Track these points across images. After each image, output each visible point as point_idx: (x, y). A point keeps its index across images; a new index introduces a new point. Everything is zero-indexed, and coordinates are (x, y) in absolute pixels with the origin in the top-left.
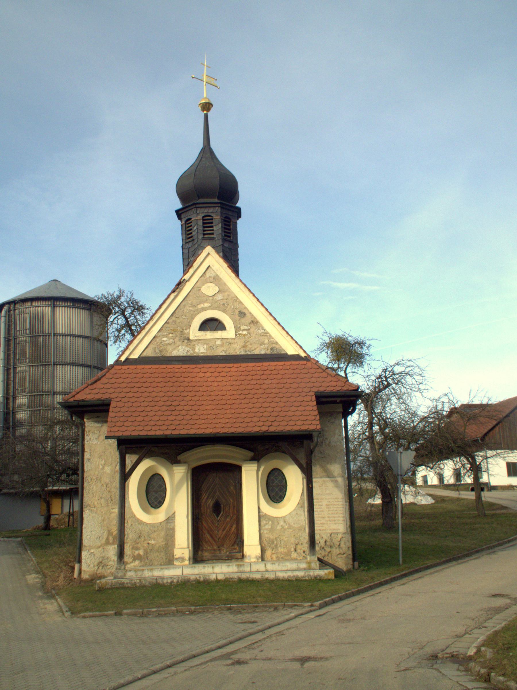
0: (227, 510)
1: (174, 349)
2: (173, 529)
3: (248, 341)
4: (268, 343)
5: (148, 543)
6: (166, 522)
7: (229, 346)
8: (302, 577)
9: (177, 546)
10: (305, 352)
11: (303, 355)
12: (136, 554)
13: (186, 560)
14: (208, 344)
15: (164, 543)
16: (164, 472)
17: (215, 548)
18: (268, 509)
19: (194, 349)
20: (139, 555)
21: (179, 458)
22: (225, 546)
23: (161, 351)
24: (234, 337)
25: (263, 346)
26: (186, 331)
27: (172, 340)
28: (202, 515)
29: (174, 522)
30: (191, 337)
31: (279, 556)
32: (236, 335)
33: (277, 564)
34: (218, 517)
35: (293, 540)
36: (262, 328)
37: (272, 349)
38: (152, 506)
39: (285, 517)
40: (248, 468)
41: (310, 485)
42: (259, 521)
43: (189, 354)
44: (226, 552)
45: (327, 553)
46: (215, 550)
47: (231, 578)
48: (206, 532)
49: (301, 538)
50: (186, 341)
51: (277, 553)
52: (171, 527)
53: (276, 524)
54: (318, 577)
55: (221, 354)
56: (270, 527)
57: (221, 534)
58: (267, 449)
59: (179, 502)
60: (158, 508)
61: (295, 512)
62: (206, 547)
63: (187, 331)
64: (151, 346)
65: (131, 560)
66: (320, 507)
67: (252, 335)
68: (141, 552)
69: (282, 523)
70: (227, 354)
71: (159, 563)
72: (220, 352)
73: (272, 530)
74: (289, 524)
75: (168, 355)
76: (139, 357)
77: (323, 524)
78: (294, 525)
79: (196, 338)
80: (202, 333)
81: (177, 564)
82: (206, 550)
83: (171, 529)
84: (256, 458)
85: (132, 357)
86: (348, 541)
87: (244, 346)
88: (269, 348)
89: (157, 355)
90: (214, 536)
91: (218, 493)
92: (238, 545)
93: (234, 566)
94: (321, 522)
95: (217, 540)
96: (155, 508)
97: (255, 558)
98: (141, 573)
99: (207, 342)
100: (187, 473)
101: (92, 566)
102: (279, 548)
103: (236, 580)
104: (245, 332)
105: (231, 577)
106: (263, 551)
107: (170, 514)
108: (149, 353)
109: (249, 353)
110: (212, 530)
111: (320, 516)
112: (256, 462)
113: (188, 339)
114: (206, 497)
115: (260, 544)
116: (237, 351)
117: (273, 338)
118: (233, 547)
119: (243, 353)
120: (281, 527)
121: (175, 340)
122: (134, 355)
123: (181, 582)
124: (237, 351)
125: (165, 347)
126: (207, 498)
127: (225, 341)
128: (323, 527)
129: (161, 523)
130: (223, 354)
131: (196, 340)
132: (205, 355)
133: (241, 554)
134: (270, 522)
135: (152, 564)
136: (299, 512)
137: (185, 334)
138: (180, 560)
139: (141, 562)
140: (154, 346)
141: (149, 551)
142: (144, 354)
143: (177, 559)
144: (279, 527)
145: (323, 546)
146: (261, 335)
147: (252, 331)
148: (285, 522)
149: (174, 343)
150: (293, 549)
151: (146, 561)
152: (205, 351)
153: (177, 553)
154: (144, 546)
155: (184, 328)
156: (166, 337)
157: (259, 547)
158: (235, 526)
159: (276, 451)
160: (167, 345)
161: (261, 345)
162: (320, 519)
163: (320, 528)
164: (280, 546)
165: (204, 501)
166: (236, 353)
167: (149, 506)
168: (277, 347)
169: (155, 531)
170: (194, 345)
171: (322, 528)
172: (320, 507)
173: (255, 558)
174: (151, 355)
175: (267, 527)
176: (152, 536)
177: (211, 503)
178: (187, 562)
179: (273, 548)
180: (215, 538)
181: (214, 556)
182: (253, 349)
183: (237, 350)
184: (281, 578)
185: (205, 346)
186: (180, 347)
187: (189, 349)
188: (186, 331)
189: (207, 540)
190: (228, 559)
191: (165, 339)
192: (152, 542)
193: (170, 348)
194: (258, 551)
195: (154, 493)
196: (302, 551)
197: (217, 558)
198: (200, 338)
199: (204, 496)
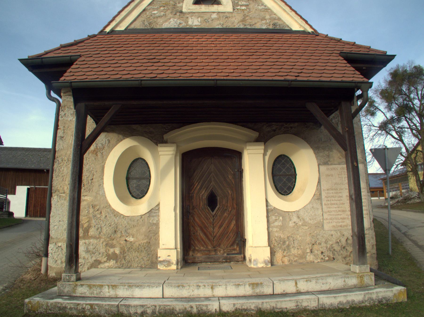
1: (166, 21)
2: (157, 225)
3: (247, 16)
4: (270, 19)
5: (126, 240)
6: (148, 215)
7: (227, 19)
8: (360, 302)
9: (161, 246)
10: (311, 27)
11: (310, 30)
12: (110, 253)
13: (172, 263)
14: (202, 17)
15: (145, 241)
16: (147, 155)
17: (210, 248)
18: (278, 202)
19: (187, 22)
20: (114, 253)
21: (166, 137)
22: (222, 246)
23: (150, 24)
24: (232, 11)
25: (263, 22)
26: (178, 5)
27: (162, 13)
28: (193, 209)
29: (159, 216)
30: (184, 10)
31: (292, 259)
32: (234, 9)
33: (314, 281)
34: (213, 211)
35: (308, 239)
36: (263, 4)
37: (274, 24)
38: (133, 196)
39: (298, 211)
40: (249, 151)
41: (355, 163)
42: (268, 217)
43: (181, 26)
44: (224, 253)
45: (349, 253)
46: (209, 251)
47: (245, 310)
48: (198, 229)
49: (319, 237)
50: (178, 14)
51: (289, 255)
52: (155, 222)
53: (288, 220)
54: (384, 301)
55: (217, 27)
56: (280, 224)
57: (217, 231)
58: (275, 131)
59: (165, 194)
60: (141, 198)
61: (311, 205)
62: (199, 247)
63: (181, 5)
64: (140, 19)
65: (105, 259)
66: (339, 199)
67: (251, 10)
68: (117, 251)
69: (295, 219)
70: (224, 26)
71: (139, 265)
72: (216, 25)
73: (282, 228)
74: (304, 220)
75: (158, 27)
76: (125, 29)
77: (344, 218)
78: (309, 222)
79: (189, 11)
80: (197, 6)
81: (161, 268)
82: (198, 251)
83: (153, 224)
84: (263, 139)
85: (118, 29)
86: (373, 238)
87: (243, 20)
88: (271, 23)
89: (146, 28)
90: (208, 234)
91: (213, 183)
92: (238, 245)
93: (247, 286)
94: (342, 216)
95: (212, 238)
96: (136, 198)
97: (262, 263)
98: (98, 290)
99: (202, 15)
100: (176, 156)
101: (59, 262)
102: (292, 250)
103: (254, 312)
104: (243, 8)
105: (245, 307)
106: (273, 253)
107: (154, 206)
108: (138, 25)
109: (249, 27)
110: (205, 227)
111: (340, 209)
112: (263, 143)
113: (181, 12)
114: (198, 187)
115: (269, 245)
116: (235, 24)
117: (275, 14)
118: (232, 248)
119: (242, 27)
120: (294, 224)
121: (167, 13)
122: (121, 27)
123: (160, 313)
124: (235, 24)
125: (155, 20)
126: (200, 188)
127: (221, 15)
128: (344, 222)
129: (141, 216)
130: (220, 27)
131: (190, 13)
132: (200, 27)
133: (243, 255)
134: (281, 218)
135: (131, 266)
136: (315, 205)
137: (178, 7)
138: (165, 264)
139: (117, 262)
140: (143, 19)
141: (126, 250)
142: (132, 27)
143: (161, 262)
144: (291, 224)
145: (344, 245)
146: (261, 10)
147: (251, 6)
148: (298, 217)
149: (165, 15)
150: (308, 251)
151: (123, 262)
152: (199, 24)
153: (162, 255)
154: (120, 244)
155: (177, 2)
156: (157, 10)
157: (269, 248)
158: (234, 222)
159: (285, 133)
160: (157, 18)
161: (262, 20)
162: (340, 213)
163: (341, 224)
164: (293, 247)
165: (196, 192)
166: (235, 26)
167: (130, 196)
168: (280, 22)
169: (134, 226)
170: (187, 18)
171: (344, 224)
172: (339, 199)
173: (262, 263)
174: (139, 28)
175: (276, 224)
176: (130, 231)
177: (204, 194)
178: (174, 267)
179: (285, 250)
180: (210, 237)
181: (209, 258)
182: (253, 23)
183: (235, 22)
184: (327, 307)
185: (199, 19)
186: (172, 20)
187: (181, 22)
188: (178, 5)
189: (199, 238)
190: (226, 262)
191: (155, 12)
192: (131, 239)
193: (160, 21)
194: (266, 254)
195: (135, 181)
196: (319, 253)
197: (213, 260)
198: (194, 11)
199: (197, 186)
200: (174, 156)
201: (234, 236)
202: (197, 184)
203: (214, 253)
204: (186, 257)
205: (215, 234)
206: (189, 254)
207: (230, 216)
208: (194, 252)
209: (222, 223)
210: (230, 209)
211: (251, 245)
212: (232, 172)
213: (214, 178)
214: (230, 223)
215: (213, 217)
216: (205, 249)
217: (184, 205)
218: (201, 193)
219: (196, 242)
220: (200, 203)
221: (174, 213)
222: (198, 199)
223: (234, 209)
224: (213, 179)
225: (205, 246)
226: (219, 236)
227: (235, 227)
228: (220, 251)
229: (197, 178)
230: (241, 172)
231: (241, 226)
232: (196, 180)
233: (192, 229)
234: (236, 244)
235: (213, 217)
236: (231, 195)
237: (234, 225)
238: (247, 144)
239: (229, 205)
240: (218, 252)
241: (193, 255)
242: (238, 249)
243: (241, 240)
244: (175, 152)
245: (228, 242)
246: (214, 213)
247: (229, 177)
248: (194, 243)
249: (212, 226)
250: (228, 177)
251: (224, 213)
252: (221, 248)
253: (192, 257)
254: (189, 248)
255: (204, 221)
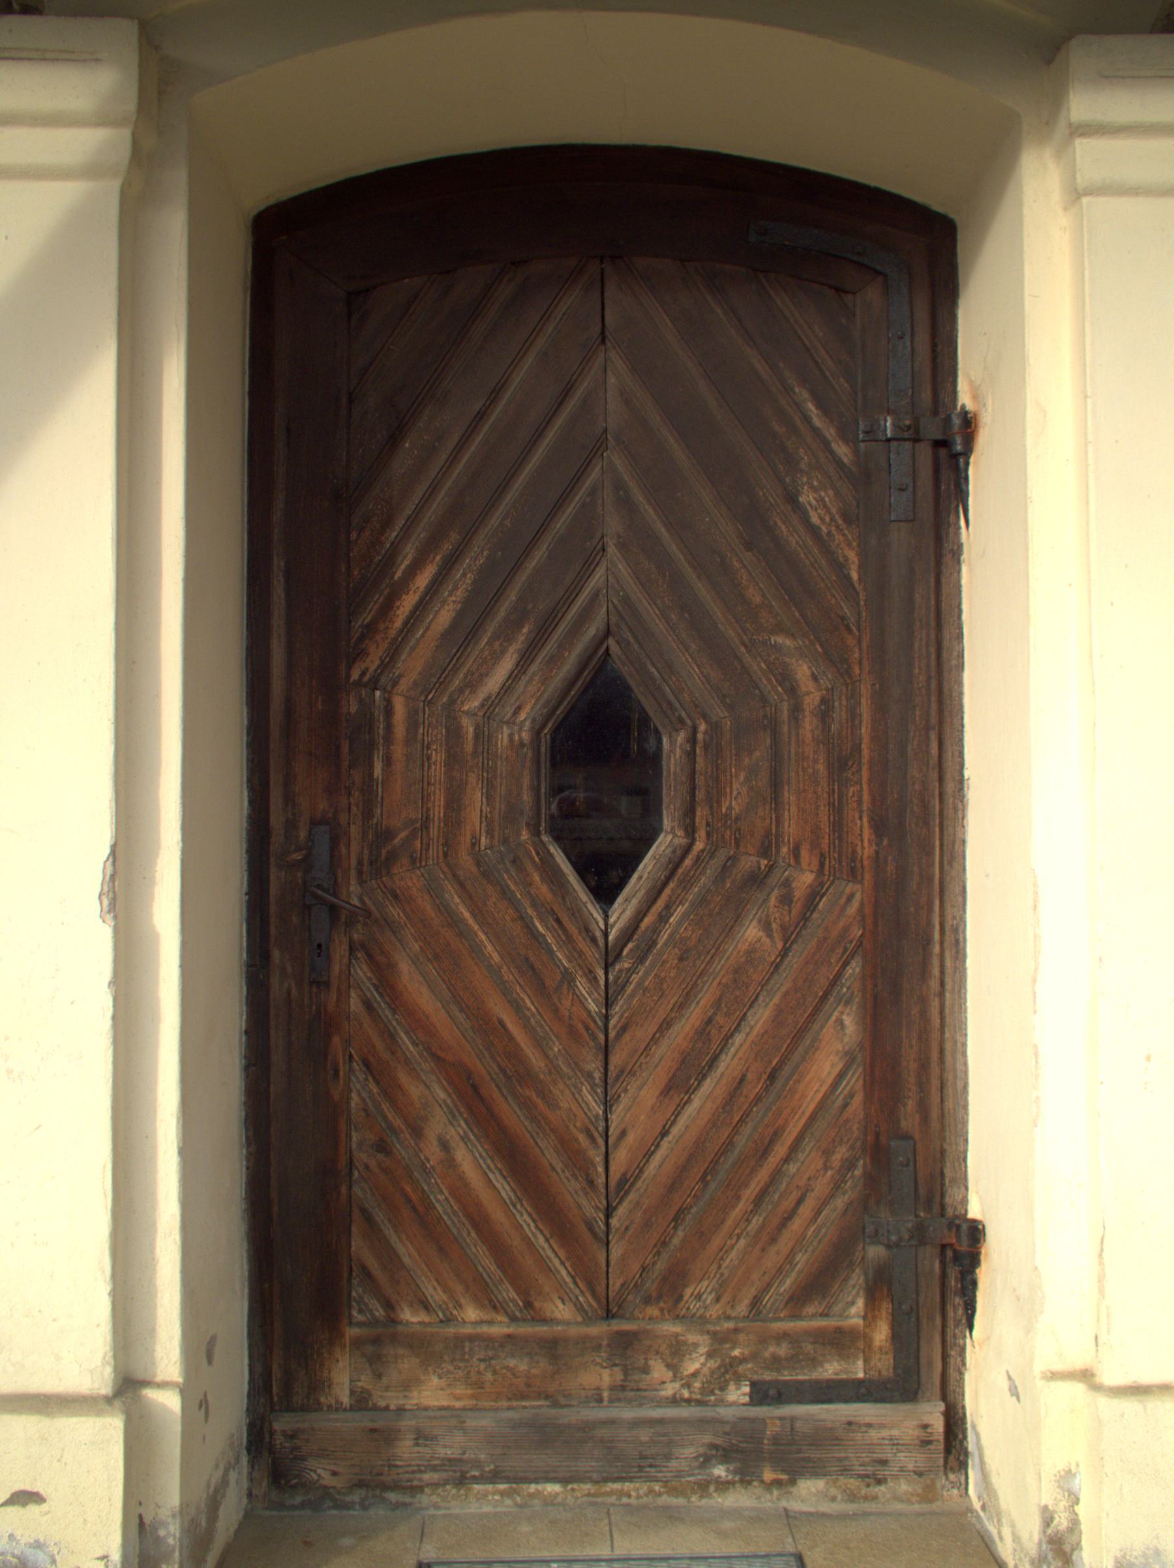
0: (735, 801)
22: (700, 1293)
28: (380, 861)
34: (606, 894)
44: (727, 1372)
46: (552, 1347)
48: (428, 1092)
82: (423, 1347)
90: (549, 1156)
91: (614, 571)
92: (879, 1286)
95: (590, 1207)
110: (517, 1073)
114: (443, 616)
126: (464, 633)
133: (933, 1415)
158: (843, 1028)
165: (413, 665)
177: (511, 696)
180: (568, 1188)
181: (545, 1435)
189: (442, 1203)
199: (427, 601)
200: (112, 188)
201: (837, 1187)
202: (422, 581)
203: (606, 1377)
204: (282, 1423)
205: (621, 1158)
206: (317, 1385)
207: (794, 961)
208: (376, 1363)
209: (702, 1033)
210: (808, 878)
211: (1059, 1339)
212: (843, 451)
213: (626, 504)
214: (799, 1035)
215: (610, 958)
216: (500, 1328)
217: (276, 820)
218: (471, 685)
219: (406, 1251)
220: (455, 803)
221: (99, 939)
222: (438, 756)
223: (854, 874)
224: (613, 525)
225: (508, 1293)
226: (674, 1185)
227: (855, 1080)
228: (677, 1351)
229: (432, 514)
230: (939, 452)
231: (924, 1066)
232: (421, 533)
233: (359, 1092)
234: (857, 1279)
235: (610, 958)
236: (824, 713)
237: (850, 1059)
238: (1081, 54)
239: (791, 828)
240: (659, 1371)
241: (361, 1402)
242: (881, 1334)
243: (920, 1234)
244: (122, 137)
245: (772, 1259)
246: (622, 911)
247: (807, 498)
248: (390, 1259)
249: (594, 1066)
250: (792, 499)
251: (738, 919)
252: (699, 1322)
253: (352, 1423)
254: (329, 1307)
255: (499, 1009)
